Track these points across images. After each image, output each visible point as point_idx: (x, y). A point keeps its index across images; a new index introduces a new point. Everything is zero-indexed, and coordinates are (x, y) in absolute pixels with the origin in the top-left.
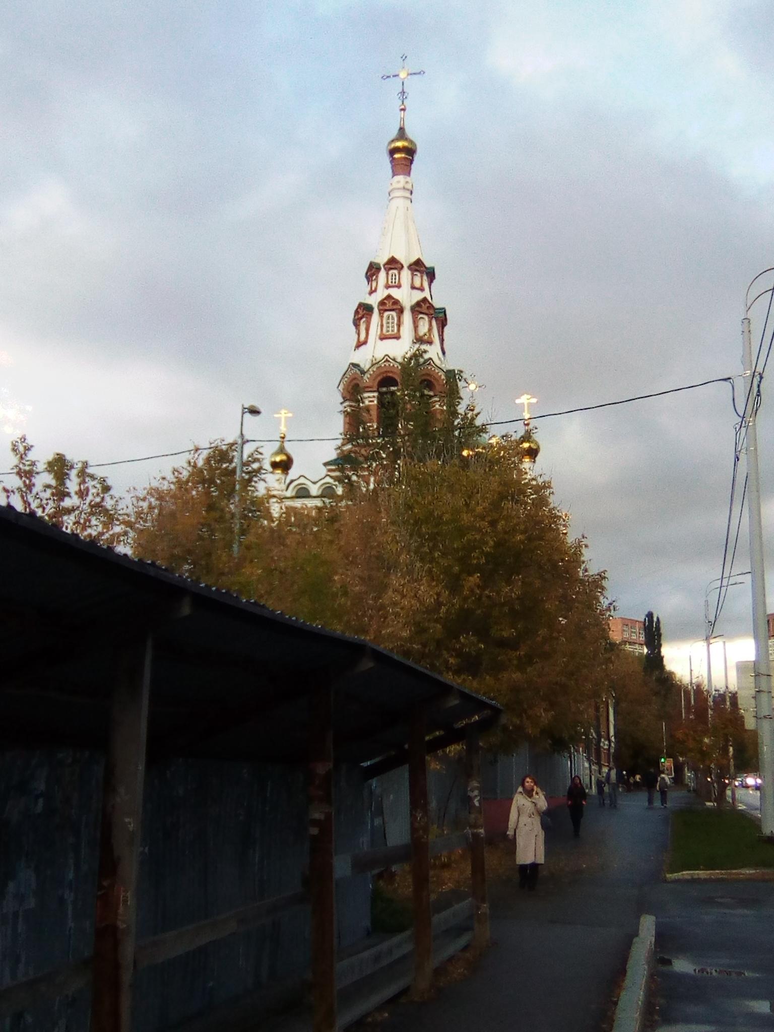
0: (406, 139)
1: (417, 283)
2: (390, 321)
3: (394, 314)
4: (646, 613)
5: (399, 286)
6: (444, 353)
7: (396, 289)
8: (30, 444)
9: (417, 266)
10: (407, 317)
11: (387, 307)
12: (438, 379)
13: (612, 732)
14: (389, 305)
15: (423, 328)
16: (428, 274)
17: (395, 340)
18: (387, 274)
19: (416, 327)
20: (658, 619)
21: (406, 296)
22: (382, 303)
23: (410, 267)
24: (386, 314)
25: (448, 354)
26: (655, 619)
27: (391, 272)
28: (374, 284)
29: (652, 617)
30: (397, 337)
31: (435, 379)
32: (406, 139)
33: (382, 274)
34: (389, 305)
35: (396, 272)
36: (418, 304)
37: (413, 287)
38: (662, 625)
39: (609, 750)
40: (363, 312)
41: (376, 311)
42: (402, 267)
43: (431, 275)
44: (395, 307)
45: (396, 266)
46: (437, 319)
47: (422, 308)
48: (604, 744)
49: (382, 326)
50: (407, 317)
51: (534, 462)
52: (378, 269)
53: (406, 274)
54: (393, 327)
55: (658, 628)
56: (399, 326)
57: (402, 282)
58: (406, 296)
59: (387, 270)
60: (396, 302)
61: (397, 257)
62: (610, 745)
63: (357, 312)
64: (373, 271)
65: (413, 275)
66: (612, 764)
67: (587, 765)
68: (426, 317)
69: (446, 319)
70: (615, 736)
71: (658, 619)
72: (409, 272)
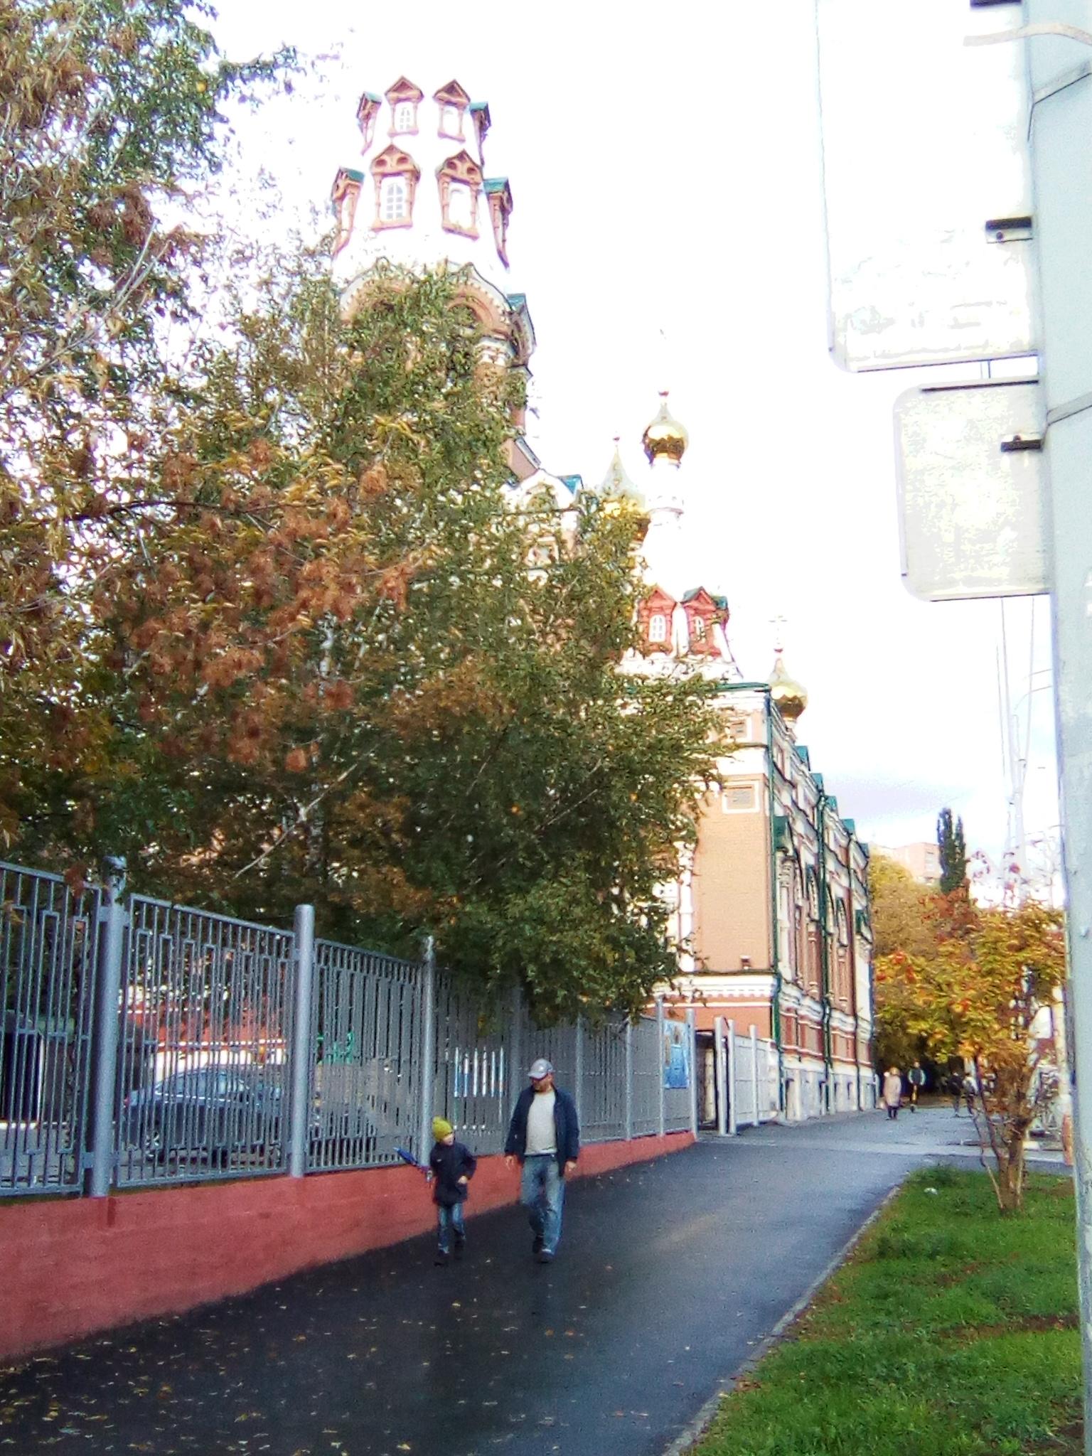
0: (673, 424)
2: (395, 196)
8: (463, 263)
14: (392, 164)
16: (474, 112)
17: (469, 240)
18: (394, 110)
23: (436, 97)
24: (388, 181)
25: (527, 266)
27: (400, 106)
31: (482, 306)
32: (673, 424)
34: (392, 164)
40: (349, 181)
42: (422, 95)
54: (390, 200)
55: (960, 836)
64: (368, 107)
67: (773, 1059)
69: (510, 199)
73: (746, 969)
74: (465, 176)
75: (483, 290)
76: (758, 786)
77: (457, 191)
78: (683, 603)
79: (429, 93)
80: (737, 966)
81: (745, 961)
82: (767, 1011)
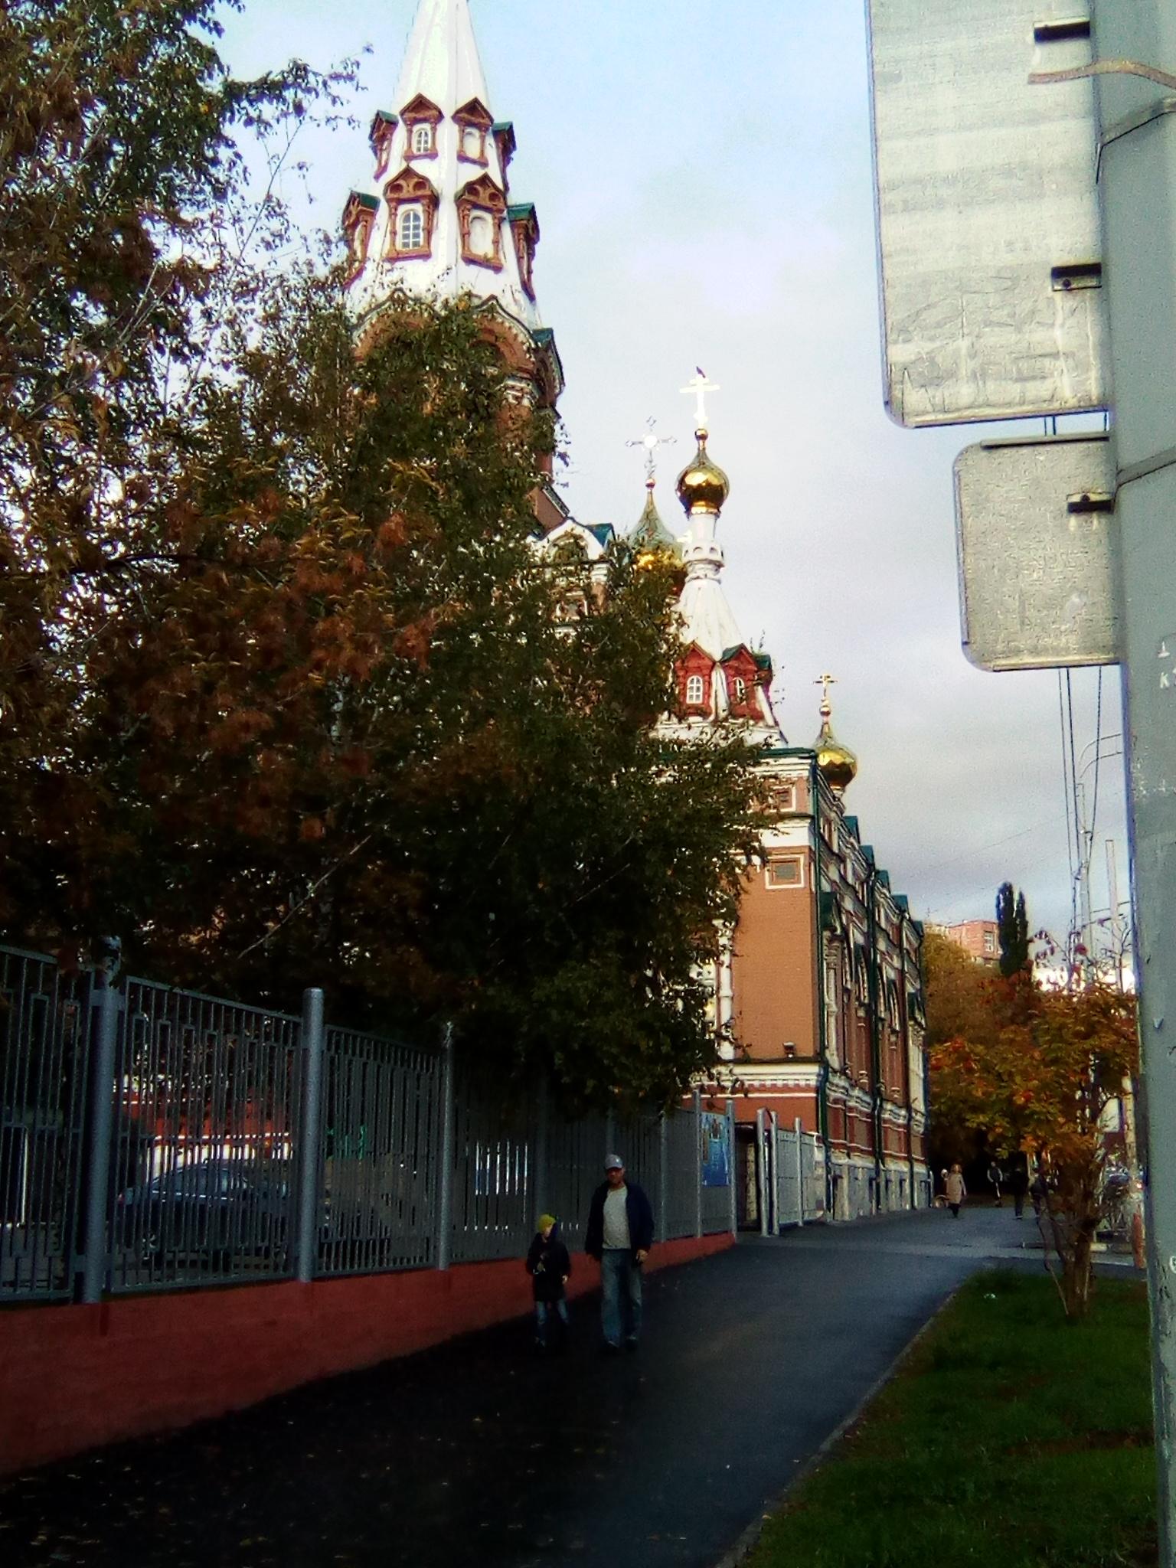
1: (473, 151)
3: (418, 208)
4: (1000, 885)
5: (432, 155)
6: (531, 297)
7: (427, 161)
9: (473, 114)
10: (447, 214)
11: (404, 194)
12: (510, 341)
13: (917, 1091)
14: (408, 190)
15: (482, 241)
16: (497, 134)
18: (410, 132)
19: (465, 235)
20: (1021, 896)
21: (447, 175)
22: (394, 186)
23: (456, 118)
24: (403, 209)
26: (1016, 897)
27: (417, 128)
28: (384, 156)
29: (1011, 893)
30: (426, 256)
33: (400, 134)
35: (427, 126)
36: (470, 188)
37: (462, 158)
38: (1028, 908)
39: (908, 1127)
41: (383, 208)
43: (506, 140)
44: (419, 193)
45: (428, 113)
46: (513, 224)
47: (482, 196)
48: (894, 1115)
49: (394, 233)
50: (447, 214)
51: (717, 515)
52: (392, 124)
53: (448, 131)
55: (1022, 912)
56: (429, 233)
57: (439, 147)
58: (447, 175)
59: (411, 123)
60: (422, 182)
61: (432, 96)
62: (910, 1118)
63: (347, 213)
64: (382, 129)
65: (463, 135)
66: (917, 1155)
68: (488, 217)
70: (929, 1097)
71: (1021, 896)
72: (456, 128)
73: (790, 1056)
74: (489, 204)
75: (507, 324)
76: (802, 859)
77: (470, 134)
78: (722, 662)
79: (448, 112)
80: (780, 1053)
81: (789, 1049)
82: (813, 1102)
